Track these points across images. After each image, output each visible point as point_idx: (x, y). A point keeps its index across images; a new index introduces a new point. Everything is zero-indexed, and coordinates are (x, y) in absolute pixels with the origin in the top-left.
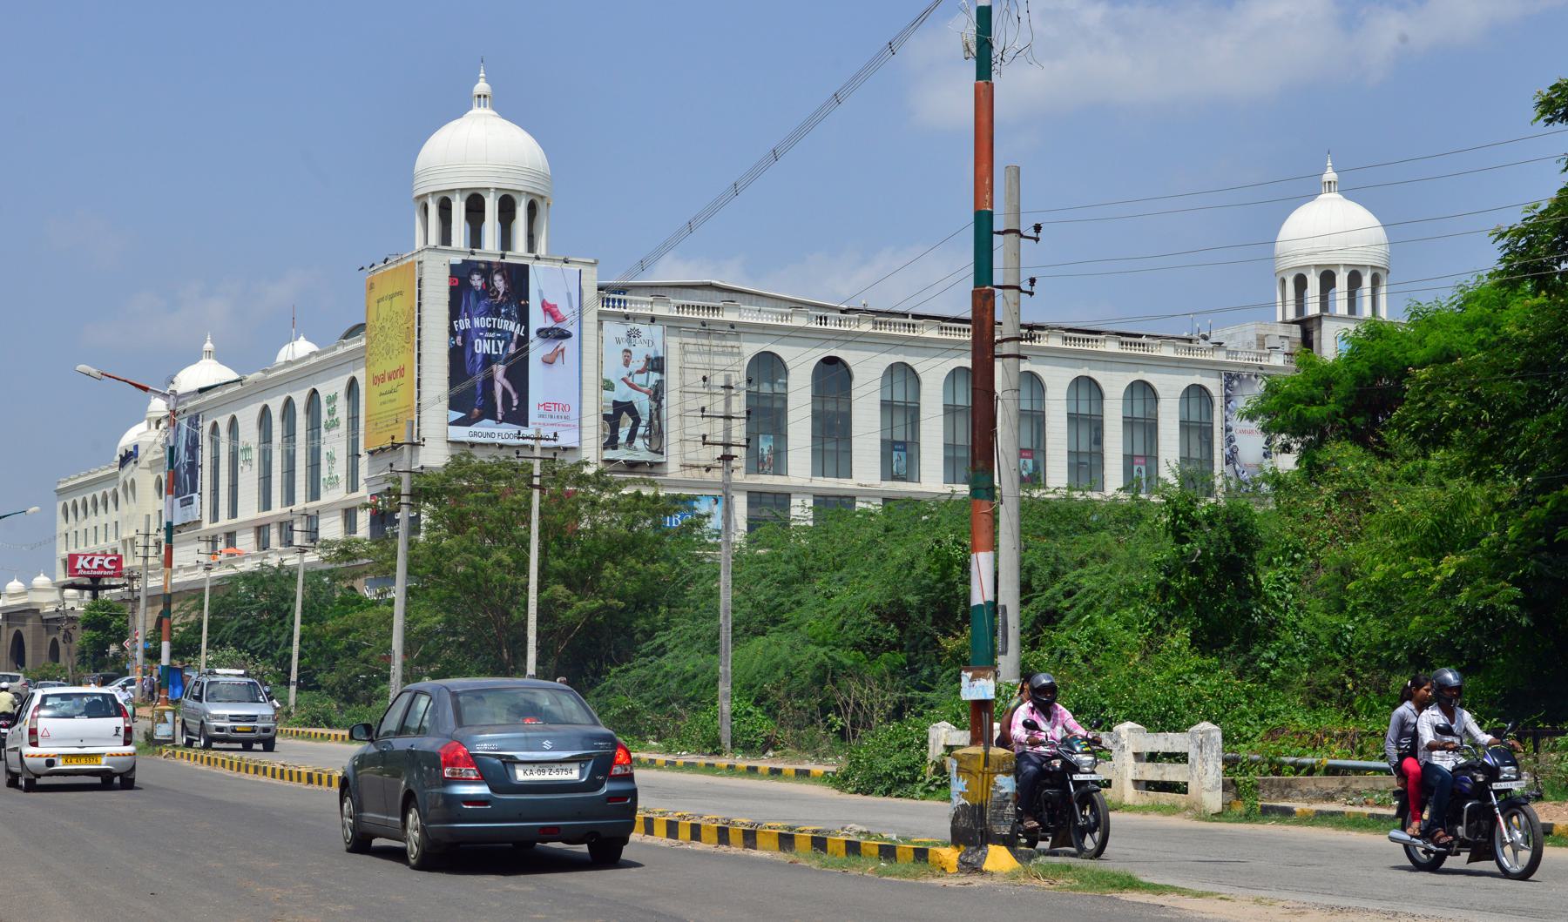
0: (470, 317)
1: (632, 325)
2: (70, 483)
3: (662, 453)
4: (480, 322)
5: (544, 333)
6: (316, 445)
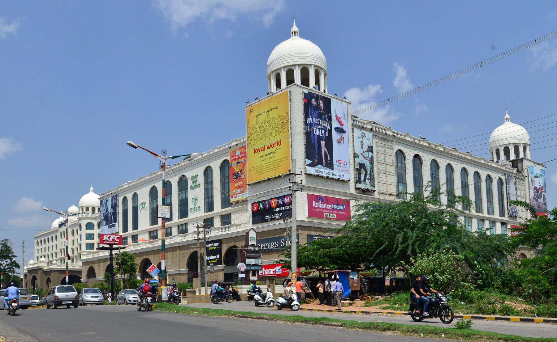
0: (312, 118)
1: (363, 131)
2: (39, 235)
3: (374, 187)
4: (316, 121)
5: (336, 129)
6: (184, 197)
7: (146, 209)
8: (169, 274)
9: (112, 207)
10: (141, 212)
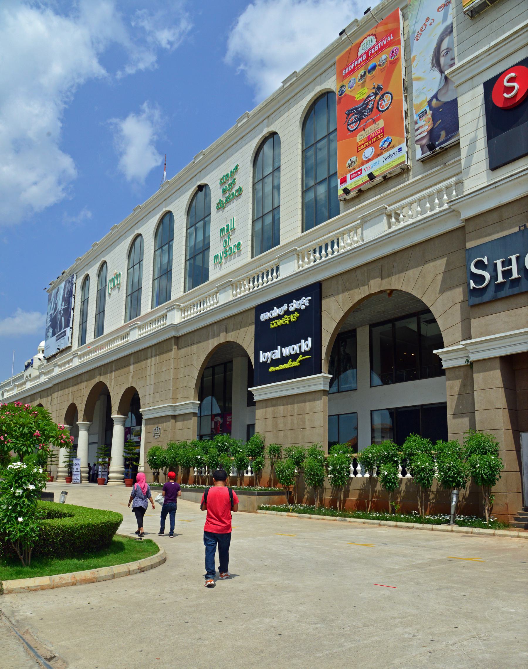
7: (119, 288)
8: (146, 420)
9: (64, 300)
10: (109, 297)
